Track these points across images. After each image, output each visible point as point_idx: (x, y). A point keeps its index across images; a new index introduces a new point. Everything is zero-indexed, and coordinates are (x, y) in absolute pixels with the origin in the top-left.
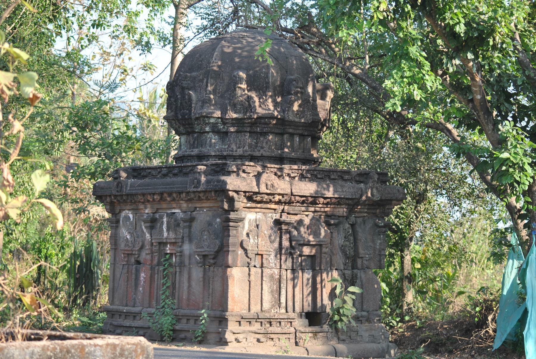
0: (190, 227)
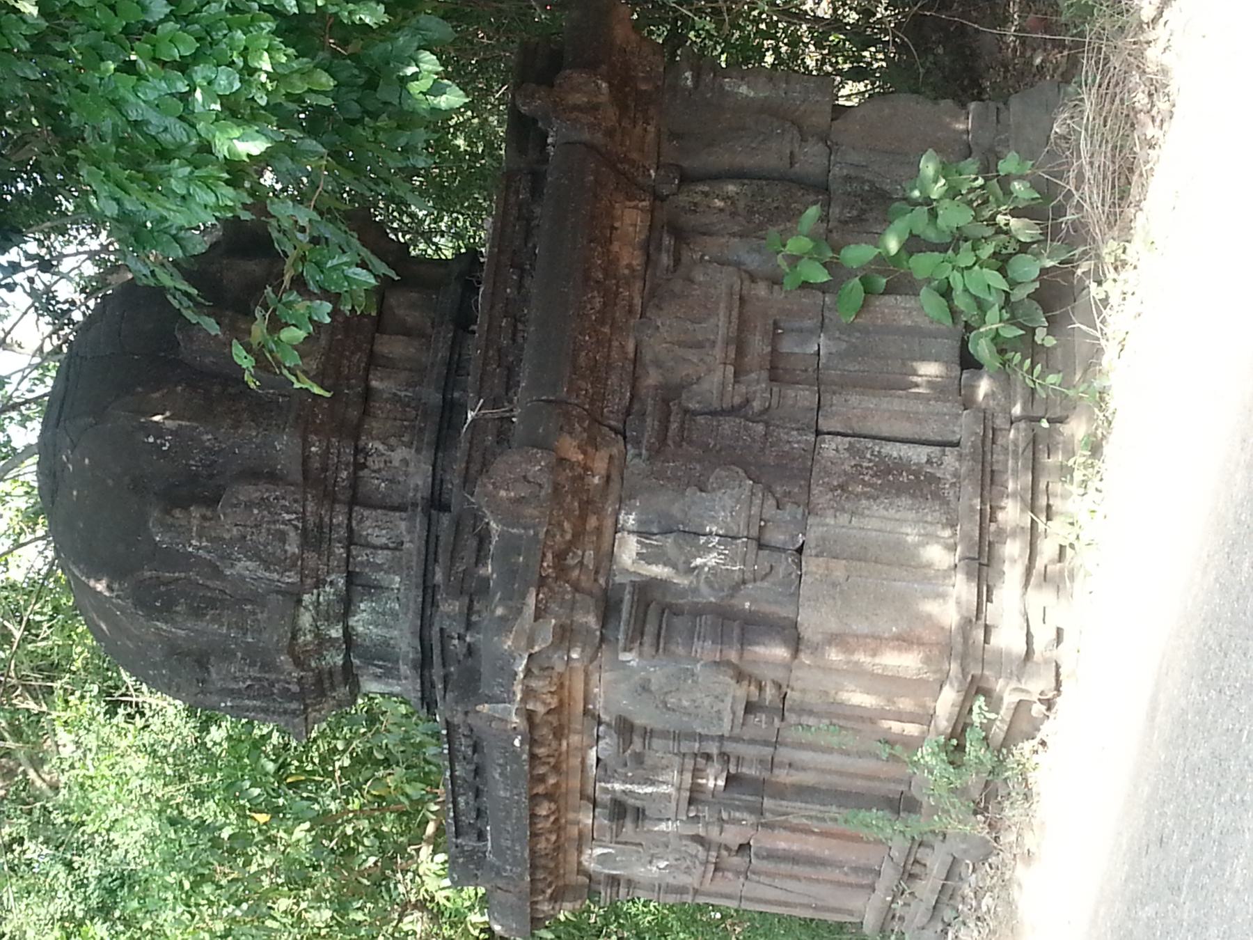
0: (648, 734)
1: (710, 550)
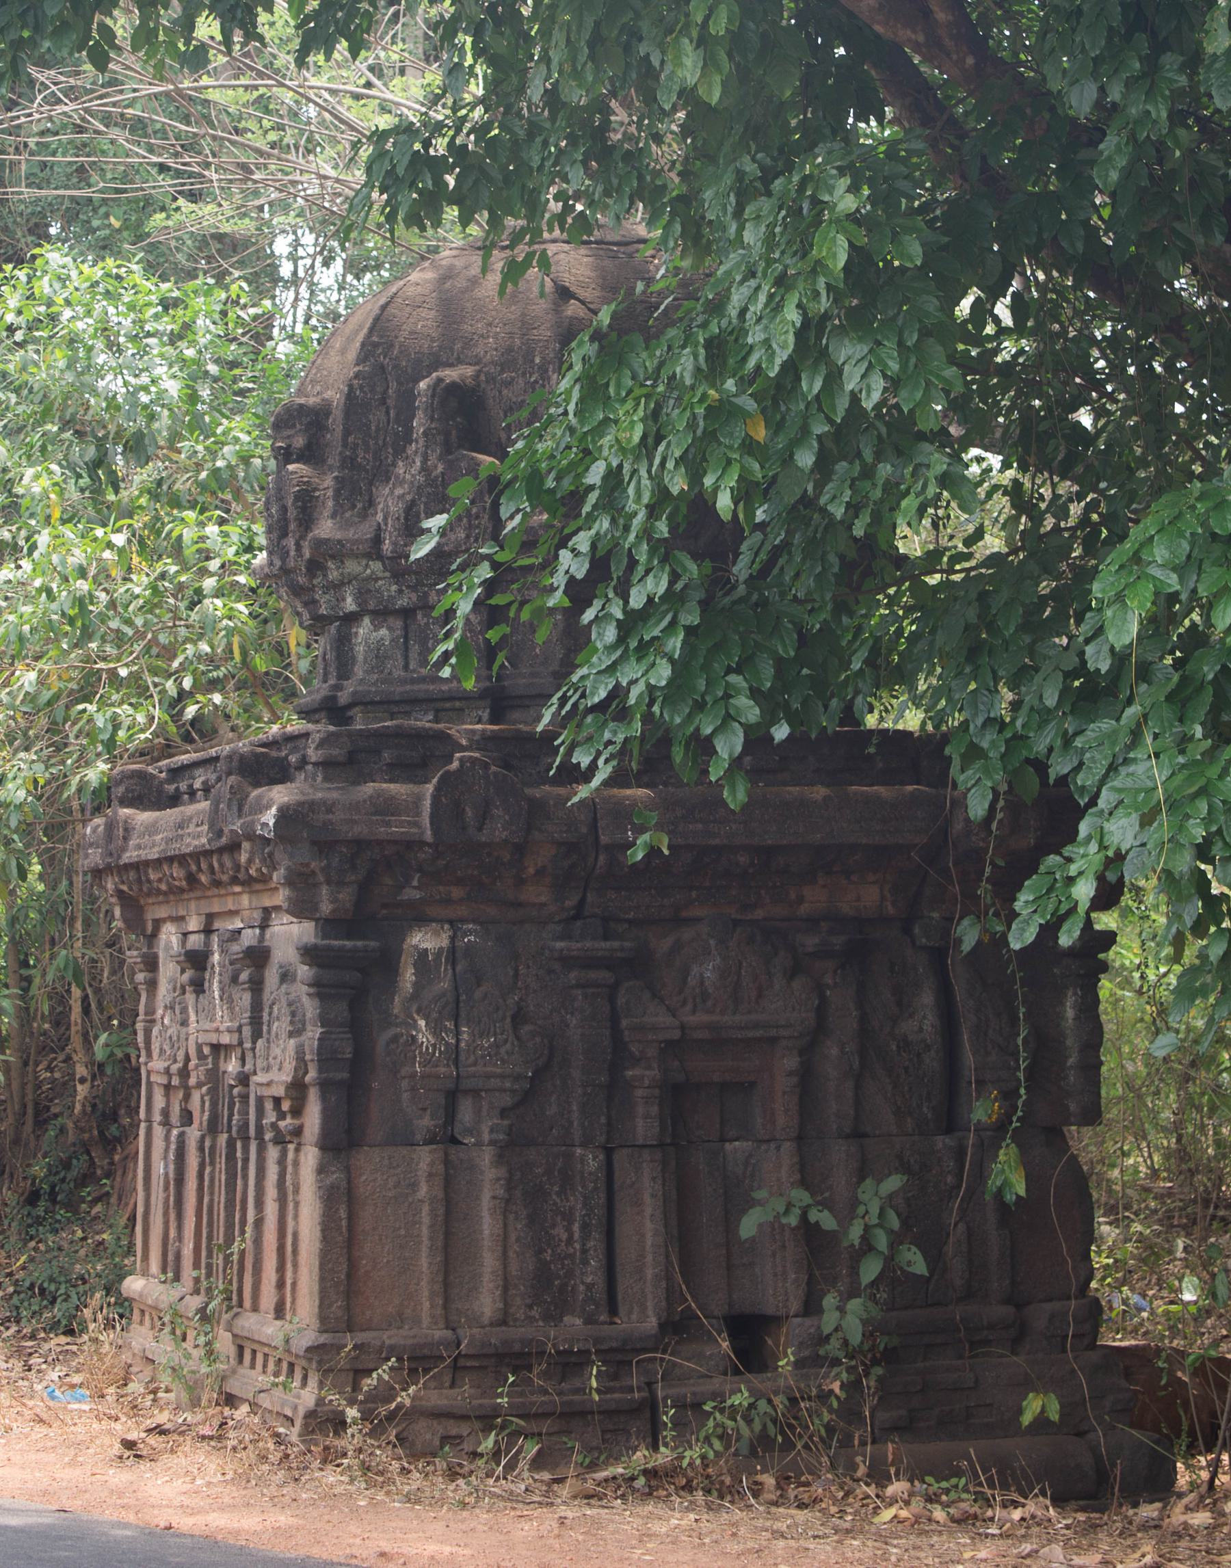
1: (435, 1034)
